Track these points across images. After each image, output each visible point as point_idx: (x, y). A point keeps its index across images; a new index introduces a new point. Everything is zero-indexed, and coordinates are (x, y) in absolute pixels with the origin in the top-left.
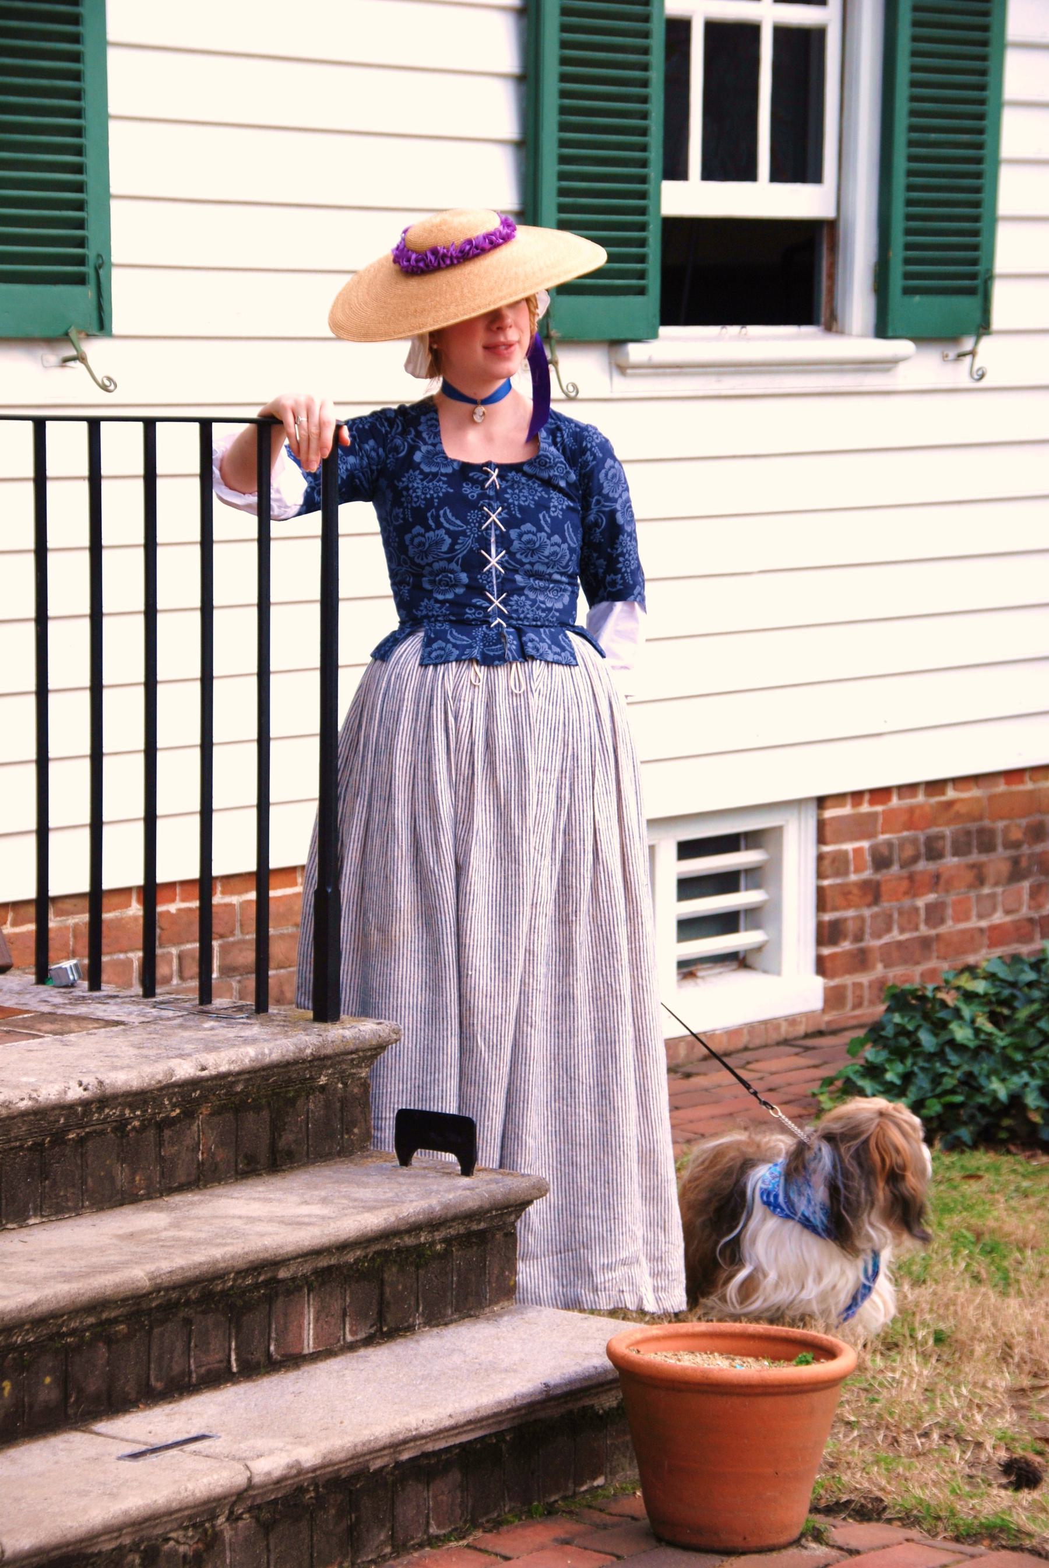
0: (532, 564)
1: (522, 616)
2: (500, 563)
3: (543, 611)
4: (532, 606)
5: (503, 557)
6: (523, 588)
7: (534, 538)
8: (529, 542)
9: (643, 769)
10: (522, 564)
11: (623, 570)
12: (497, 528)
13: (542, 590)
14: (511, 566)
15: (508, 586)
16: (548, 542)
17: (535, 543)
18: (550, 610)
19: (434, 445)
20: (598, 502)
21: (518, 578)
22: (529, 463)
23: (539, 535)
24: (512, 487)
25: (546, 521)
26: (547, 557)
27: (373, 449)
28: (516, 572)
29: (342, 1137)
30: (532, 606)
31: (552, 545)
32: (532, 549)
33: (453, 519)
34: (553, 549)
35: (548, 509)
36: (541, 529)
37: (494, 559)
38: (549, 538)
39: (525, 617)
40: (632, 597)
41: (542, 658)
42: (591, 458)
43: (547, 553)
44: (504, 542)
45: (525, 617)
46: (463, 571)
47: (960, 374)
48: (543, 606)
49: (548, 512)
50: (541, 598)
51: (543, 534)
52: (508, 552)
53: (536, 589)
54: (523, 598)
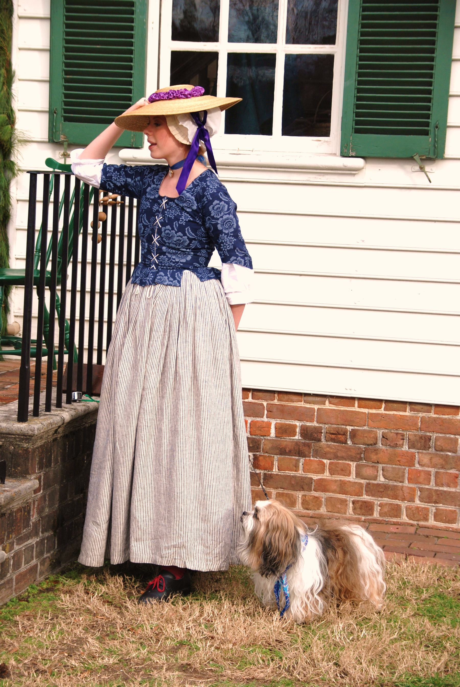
0: (169, 243)
1: (163, 265)
2: (157, 241)
3: (174, 263)
4: (168, 260)
5: (158, 238)
6: (165, 253)
7: (170, 232)
8: (168, 234)
9: (238, 335)
10: (166, 243)
11: (224, 249)
12: (158, 226)
13: (174, 254)
14: (162, 243)
15: (160, 252)
16: (175, 235)
17: (170, 235)
18: (178, 262)
19: (157, 185)
20: (209, 219)
21: (164, 248)
22: (177, 199)
23: (172, 231)
24: (169, 209)
25: (176, 226)
26: (175, 241)
27: (138, 181)
28: (164, 246)
29: (11, 469)
30: (168, 260)
31: (177, 236)
32: (169, 237)
33: (146, 219)
34: (178, 238)
35: (178, 220)
36: (173, 229)
37: (156, 239)
38: (176, 233)
39: (165, 266)
40: (229, 262)
41: (162, 283)
42: (205, 200)
43: (175, 240)
44: (160, 232)
45: (165, 266)
46: (147, 242)
47: (419, 179)
48: (174, 261)
49: (178, 222)
50: (174, 257)
51: (174, 231)
52: (161, 237)
53: (171, 253)
54: (165, 257)
